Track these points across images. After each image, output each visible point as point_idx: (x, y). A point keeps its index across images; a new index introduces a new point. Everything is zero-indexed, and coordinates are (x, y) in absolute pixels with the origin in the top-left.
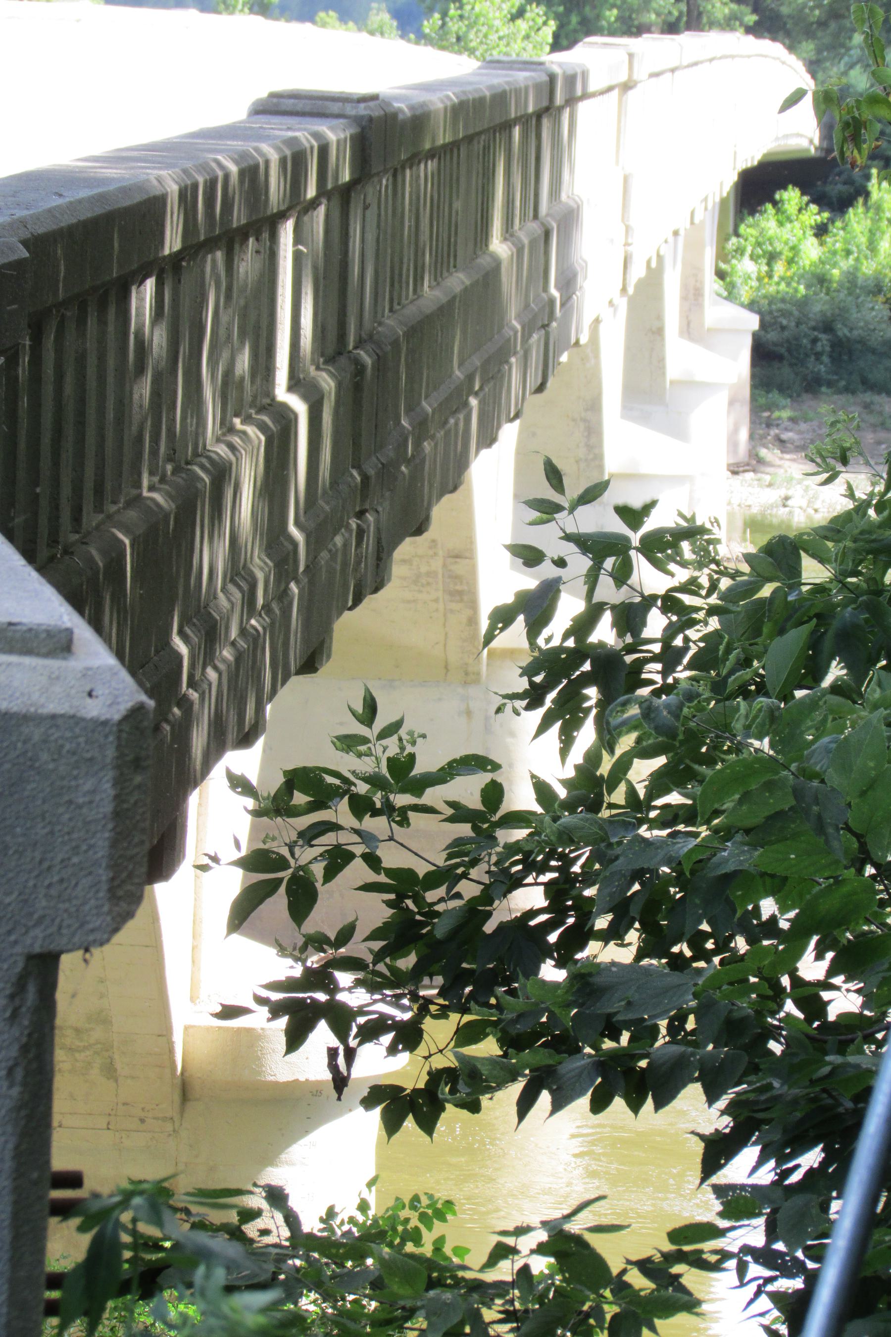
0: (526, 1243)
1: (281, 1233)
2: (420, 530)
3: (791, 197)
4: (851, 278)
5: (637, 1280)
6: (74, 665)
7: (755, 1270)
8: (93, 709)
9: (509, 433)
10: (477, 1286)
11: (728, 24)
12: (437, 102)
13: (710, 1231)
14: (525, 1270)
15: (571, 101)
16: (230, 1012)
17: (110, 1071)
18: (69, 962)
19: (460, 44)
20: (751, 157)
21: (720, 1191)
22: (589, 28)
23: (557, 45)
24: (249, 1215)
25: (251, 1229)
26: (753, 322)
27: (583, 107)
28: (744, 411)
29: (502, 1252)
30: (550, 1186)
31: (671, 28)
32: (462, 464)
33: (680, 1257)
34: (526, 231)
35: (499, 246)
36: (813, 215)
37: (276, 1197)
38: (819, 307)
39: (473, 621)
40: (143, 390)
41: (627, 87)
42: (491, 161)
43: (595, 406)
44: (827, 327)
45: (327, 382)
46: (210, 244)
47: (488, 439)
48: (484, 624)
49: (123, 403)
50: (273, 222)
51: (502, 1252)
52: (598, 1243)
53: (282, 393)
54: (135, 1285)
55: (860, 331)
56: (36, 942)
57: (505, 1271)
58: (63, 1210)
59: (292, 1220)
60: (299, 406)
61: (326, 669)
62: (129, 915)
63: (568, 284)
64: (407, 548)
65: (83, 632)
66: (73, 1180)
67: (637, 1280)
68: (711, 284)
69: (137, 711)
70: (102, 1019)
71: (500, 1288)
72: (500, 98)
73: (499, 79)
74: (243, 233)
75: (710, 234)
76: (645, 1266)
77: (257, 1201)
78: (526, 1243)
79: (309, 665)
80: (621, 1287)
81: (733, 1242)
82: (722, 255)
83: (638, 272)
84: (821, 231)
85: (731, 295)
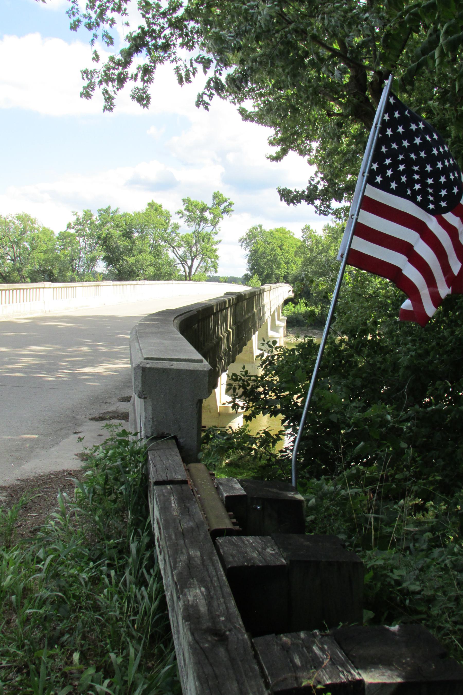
0: (261, 432)
1: (231, 432)
2: (246, 345)
3: (290, 303)
4: (298, 312)
5: (275, 437)
6: (203, 364)
7: (289, 436)
8: (205, 369)
9: (257, 333)
10: (255, 438)
11: (282, 282)
12: (247, 293)
13: (283, 431)
14: (261, 436)
15: (263, 292)
16: (224, 404)
17: (210, 412)
18: (204, 400)
19: (250, 286)
20: (286, 298)
21: (284, 426)
22: (265, 283)
23: (262, 285)
24: (227, 430)
25: (227, 432)
26: (286, 318)
27: (265, 293)
28: (285, 329)
29: (258, 433)
30: (189, 689)
31: (275, 283)
32: (251, 337)
33: (280, 434)
34: (258, 308)
35: (255, 310)
36: (293, 305)
37: (230, 427)
38: (294, 316)
39: (253, 358)
40: (212, 331)
41: (270, 290)
42: (168, 563)
43: (267, 329)
44: (296, 319)
45: (234, 328)
46: (219, 311)
47: (254, 333)
48: (255, 357)
49: (209, 332)
50: (227, 308)
51: (258, 433)
52: (270, 432)
53: (229, 329)
54: (343, 38)
55: (209, 639)
56: (199, 398)
57: (258, 436)
58: (203, 430)
59: (232, 430)
60: (231, 330)
61: (235, 363)
62: (210, 394)
63: (264, 314)
64: (245, 347)
65: (204, 360)
66: (205, 427)
67: (275, 437)
68: (281, 314)
69: (211, 369)
70: (209, 405)
71: (258, 438)
72: (255, 292)
73: (254, 290)
74: (223, 310)
75: (281, 308)
76: (276, 435)
77: (228, 428)
78: (261, 432)
79: (233, 362)
80: (273, 438)
81: (286, 432)
82: (282, 310)
83: (272, 313)
84: (294, 307)
85: (283, 315)
